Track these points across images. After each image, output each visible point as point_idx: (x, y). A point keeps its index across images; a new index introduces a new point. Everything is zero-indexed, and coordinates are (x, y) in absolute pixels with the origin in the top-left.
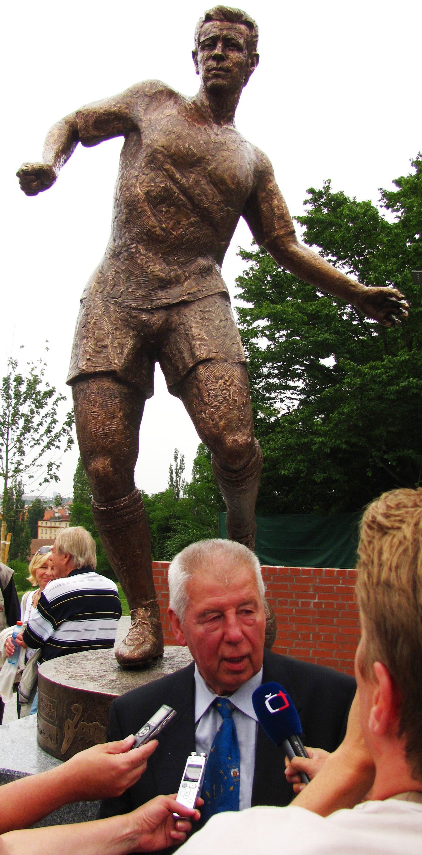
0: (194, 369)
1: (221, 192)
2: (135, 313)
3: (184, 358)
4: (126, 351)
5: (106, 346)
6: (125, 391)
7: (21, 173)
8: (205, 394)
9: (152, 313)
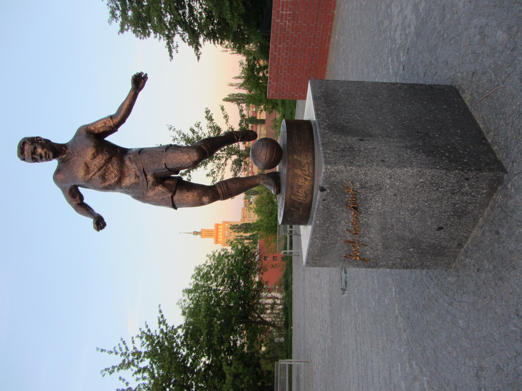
0: (169, 169)
1: (98, 155)
6: (178, 191)
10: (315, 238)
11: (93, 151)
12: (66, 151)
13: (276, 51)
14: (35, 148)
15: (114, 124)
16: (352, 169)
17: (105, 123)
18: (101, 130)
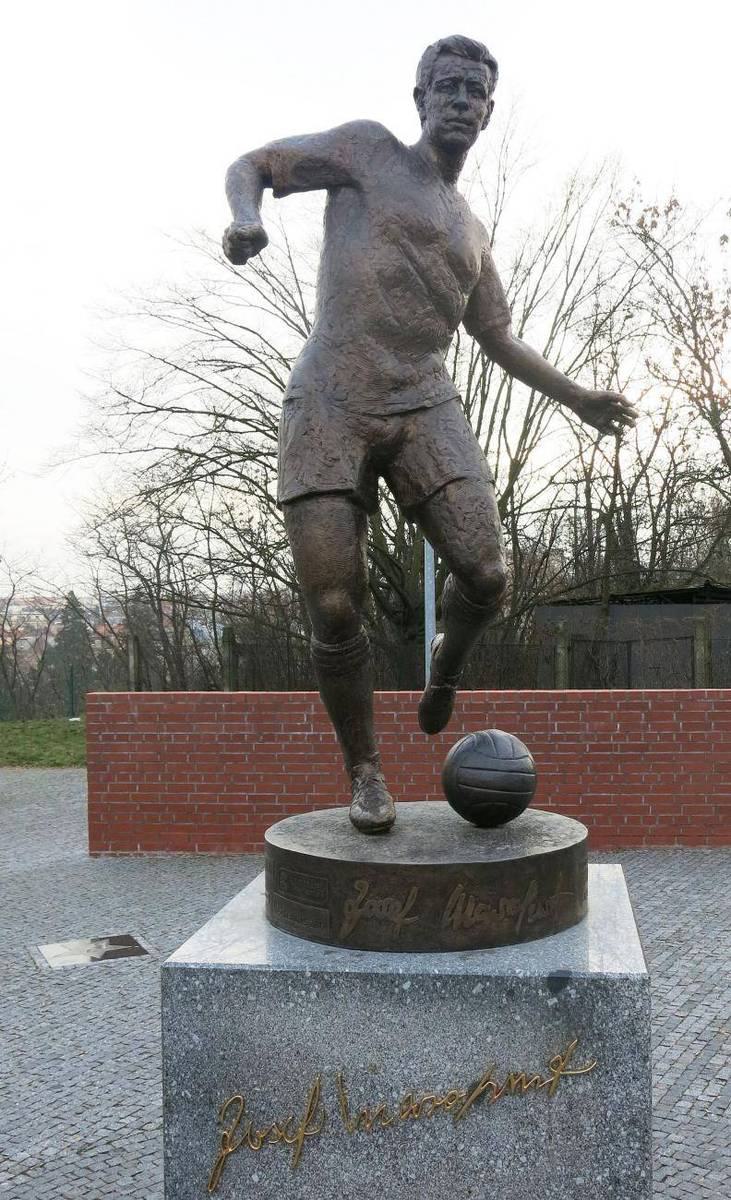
0: (443, 488)
2: (365, 419)
3: (428, 475)
5: (336, 460)
7: (235, 237)
8: (459, 519)
9: (385, 420)
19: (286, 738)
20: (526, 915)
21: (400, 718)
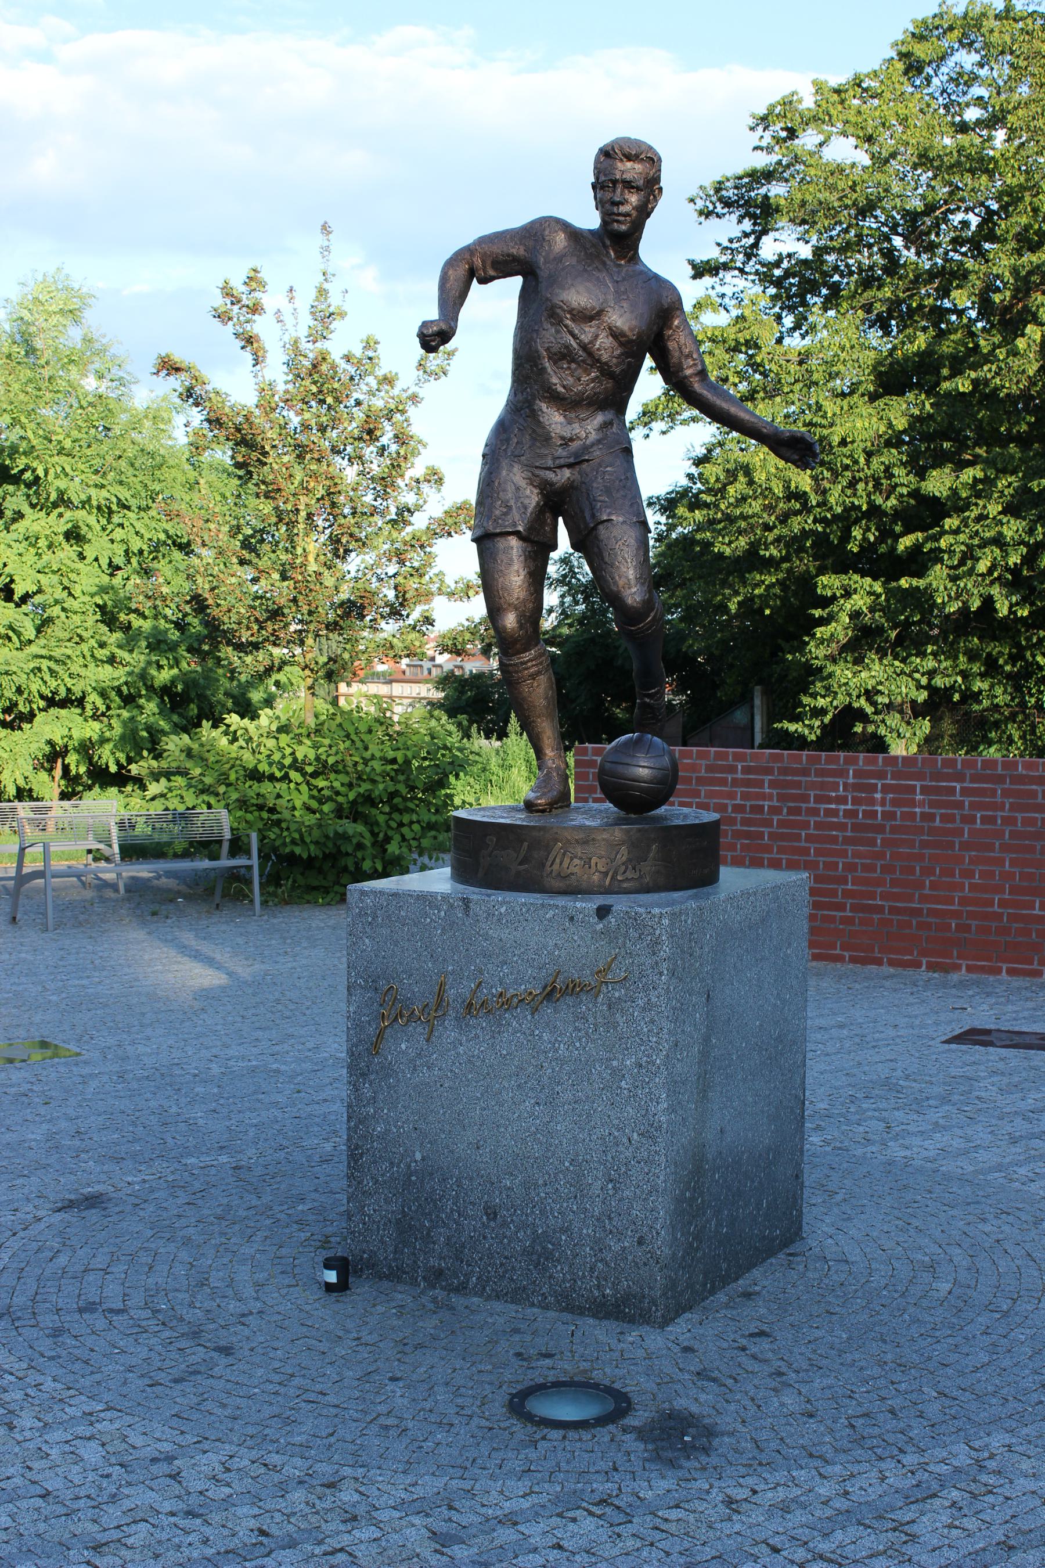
0: (595, 528)
1: (621, 344)
4: (530, 510)
10: (452, 906)
11: (629, 333)
12: (624, 258)
13: (747, 770)
14: (638, 189)
15: (686, 377)
16: (661, 974)
17: (689, 356)
18: (672, 345)
19: (815, 812)
20: (616, 873)
21: (965, 791)
